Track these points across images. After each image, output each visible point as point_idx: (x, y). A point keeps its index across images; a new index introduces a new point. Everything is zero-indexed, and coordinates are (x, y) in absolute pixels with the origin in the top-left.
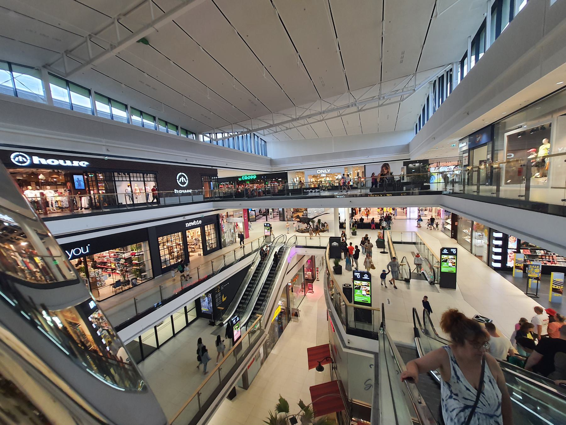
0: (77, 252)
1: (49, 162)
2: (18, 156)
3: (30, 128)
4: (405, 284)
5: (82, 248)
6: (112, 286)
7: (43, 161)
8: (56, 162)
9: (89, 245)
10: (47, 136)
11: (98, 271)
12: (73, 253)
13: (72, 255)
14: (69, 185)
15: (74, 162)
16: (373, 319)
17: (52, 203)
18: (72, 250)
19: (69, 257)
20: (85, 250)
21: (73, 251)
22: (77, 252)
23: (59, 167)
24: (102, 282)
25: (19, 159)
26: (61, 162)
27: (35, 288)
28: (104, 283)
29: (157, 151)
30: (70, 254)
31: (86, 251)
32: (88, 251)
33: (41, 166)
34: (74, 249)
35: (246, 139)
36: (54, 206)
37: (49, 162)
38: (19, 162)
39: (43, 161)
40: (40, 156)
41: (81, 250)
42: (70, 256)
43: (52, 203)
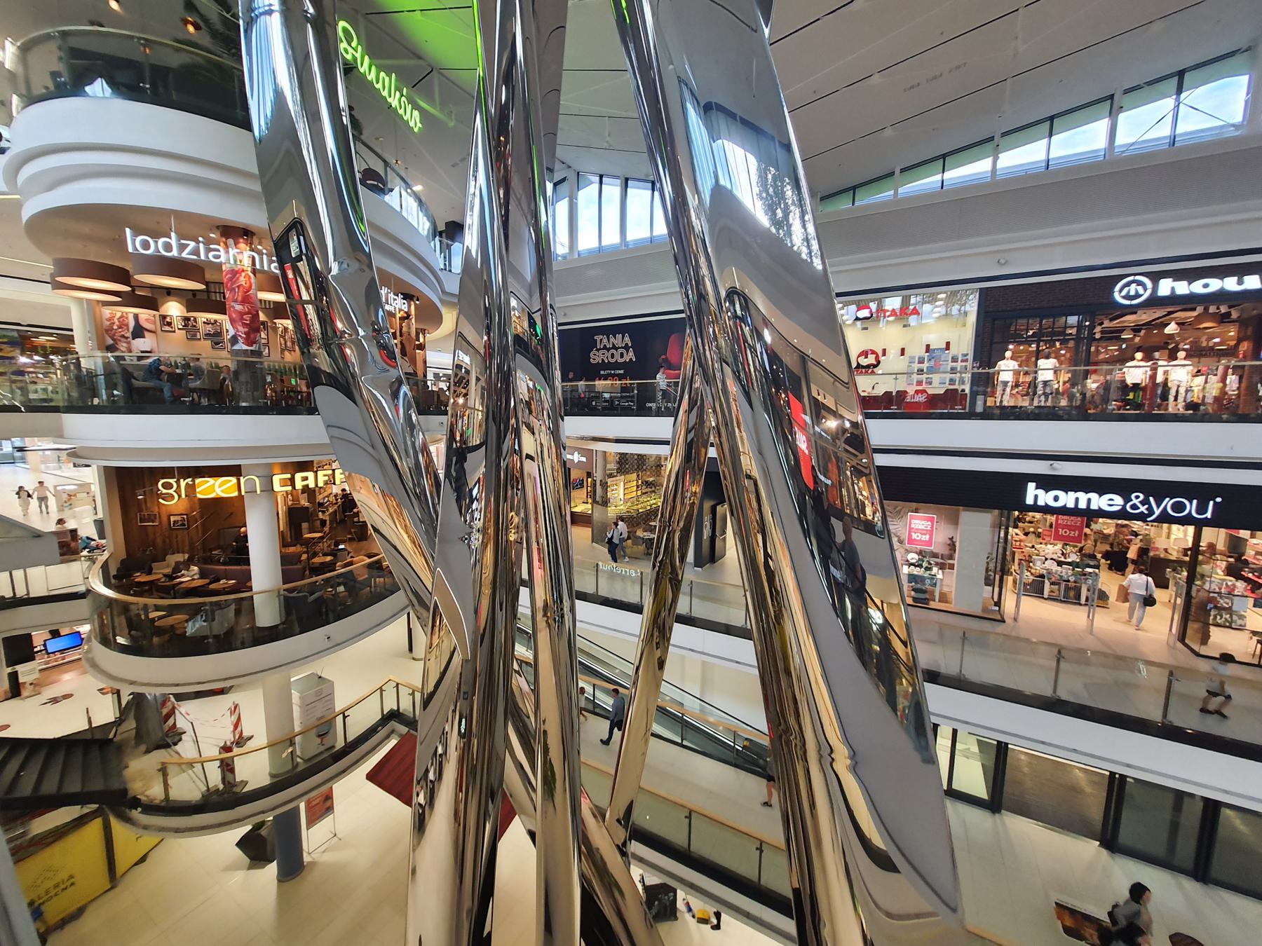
0: (1179, 507)
1: (1198, 287)
2: (1128, 284)
3: (1033, 232)
4: (13, 53)
5: (1195, 502)
6: (1255, 638)
7: (1182, 288)
8: (1215, 285)
9: (1219, 500)
10: (1111, 233)
11: (1234, 585)
12: (1165, 508)
13: (1162, 512)
14: (1245, 348)
15: (1246, 278)
16: (1257, 458)
17: (1177, 392)
18: (1167, 499)
19: (1154, 513)
20: (1202, 509)
21: (1168, 503)
22: (1179, 507)
23: (1221, 297)
24: (1235, 618)
25: (1129, 292)
26: (1231, 284)
27: (724, 108)
28: (1239, 622)
29: (934, 256)
30: (1158, 507)
31: (1206, 512)
32: (1209, 515)
33: (1174, 300)
34: (1171, 499)
35: (361, 400)
36: (1181, 399)
37: (1198, 287)
38: (1127, 297)
39: (1182, 288)
40: (1178, 275)
41: (1191, 507)
42: (1157, 512)
43: (1177, 392)
